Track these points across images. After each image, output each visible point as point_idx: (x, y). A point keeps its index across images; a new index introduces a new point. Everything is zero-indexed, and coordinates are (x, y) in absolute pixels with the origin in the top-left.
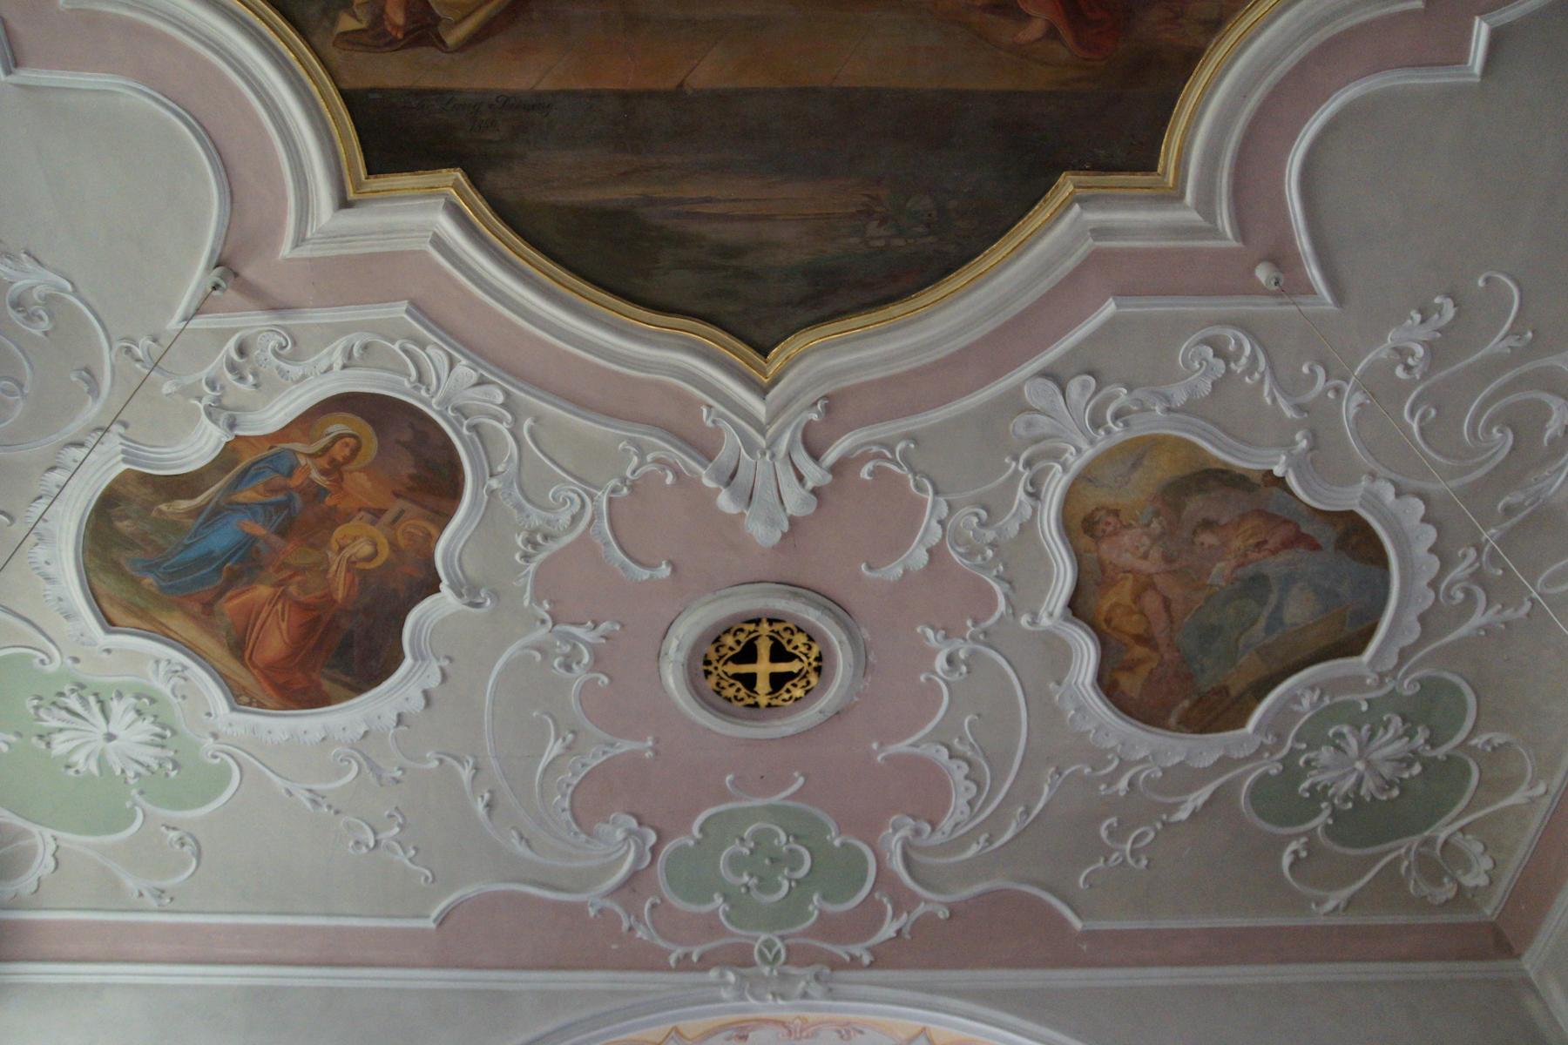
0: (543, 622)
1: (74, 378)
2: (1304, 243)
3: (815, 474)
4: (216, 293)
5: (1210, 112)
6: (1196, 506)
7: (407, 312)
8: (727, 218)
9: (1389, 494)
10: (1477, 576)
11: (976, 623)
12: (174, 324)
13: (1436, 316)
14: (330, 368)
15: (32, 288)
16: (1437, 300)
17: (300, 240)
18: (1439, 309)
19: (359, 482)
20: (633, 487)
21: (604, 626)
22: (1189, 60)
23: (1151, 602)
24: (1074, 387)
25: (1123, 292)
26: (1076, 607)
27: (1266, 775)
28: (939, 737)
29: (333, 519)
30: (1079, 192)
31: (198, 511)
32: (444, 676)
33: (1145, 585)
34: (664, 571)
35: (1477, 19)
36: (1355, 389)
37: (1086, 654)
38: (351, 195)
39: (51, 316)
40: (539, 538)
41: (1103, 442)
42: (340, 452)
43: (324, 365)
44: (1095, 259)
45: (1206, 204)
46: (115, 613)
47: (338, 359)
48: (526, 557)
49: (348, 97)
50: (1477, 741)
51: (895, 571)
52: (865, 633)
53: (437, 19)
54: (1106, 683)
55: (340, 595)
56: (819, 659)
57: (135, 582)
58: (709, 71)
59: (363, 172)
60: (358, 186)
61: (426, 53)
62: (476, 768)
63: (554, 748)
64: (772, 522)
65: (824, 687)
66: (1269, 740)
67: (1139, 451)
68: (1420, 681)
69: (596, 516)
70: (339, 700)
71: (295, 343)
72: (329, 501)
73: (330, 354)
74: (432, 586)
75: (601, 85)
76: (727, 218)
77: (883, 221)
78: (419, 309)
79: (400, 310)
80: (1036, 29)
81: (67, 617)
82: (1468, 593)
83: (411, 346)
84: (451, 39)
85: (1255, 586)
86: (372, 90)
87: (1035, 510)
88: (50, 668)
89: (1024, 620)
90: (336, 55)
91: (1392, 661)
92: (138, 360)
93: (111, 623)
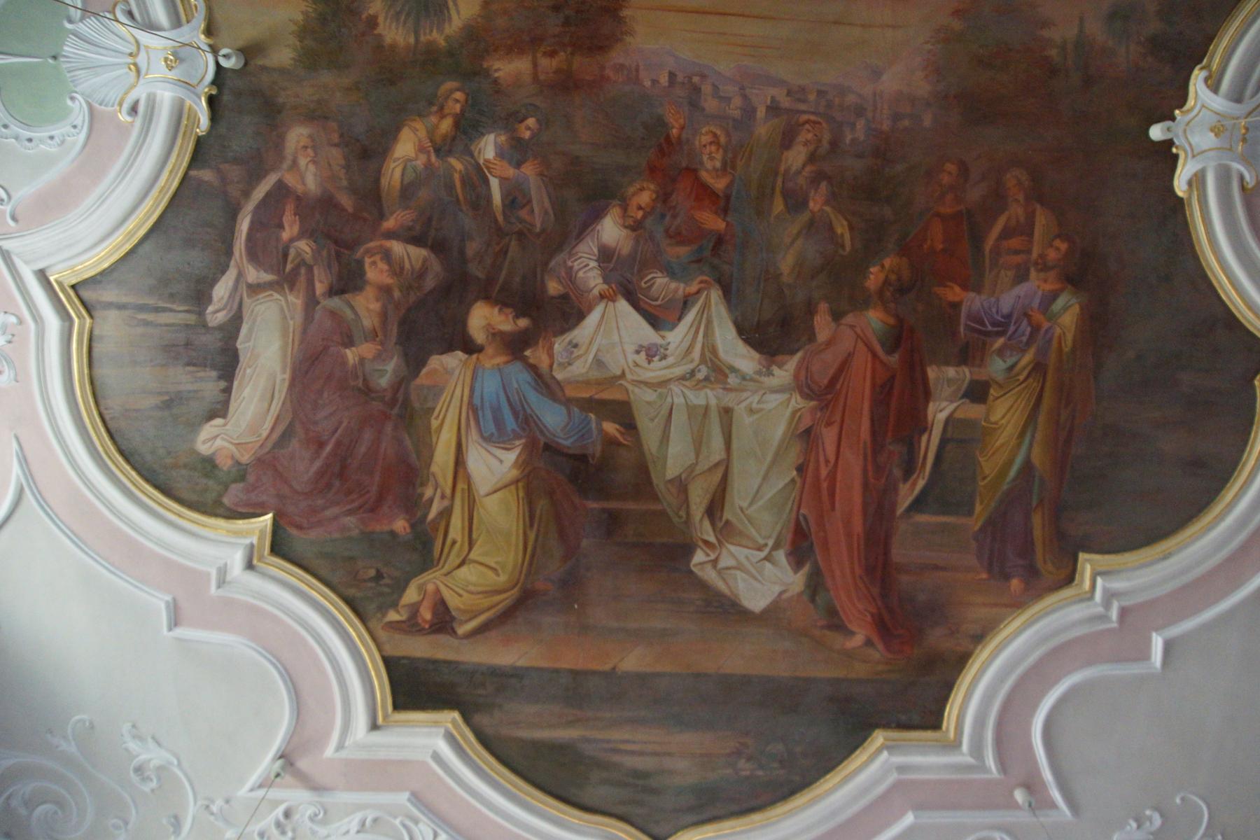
1: (164, 821)
2: (1047, 775)
4: (278, 779)
5: (975, 696)
7: (409, 800)
8: (641, 754)
13: (1148, 824)
14: (348, 832)
15: (150, 760)
16: (1148, 812)
17: (340, 746)
18: (1150, 819)
22: (962, 660)
25: (918, 807)
30: (889, 743)
35: (1154, 635)
38: (380, 720)
39: (159, 779)
43: (344, 829)
44: (897, 786)
45: (977, 749)
47: (354, 826)
49: (387, 661)
53: (453, 619)
58: (633, 661)
59: (390, 708)
60: (386, 717)
61: (443, 638)
71: (325, 813)
73: (350, 822)
75: (557, 665)
76: (641, 754)
77: (749, 759)
78: (416, 798)
79: (403, 798)
80: (858, 640)
84: (461, 630)
86: (403, 658)
90: (383, 635)
92: (212, 814)
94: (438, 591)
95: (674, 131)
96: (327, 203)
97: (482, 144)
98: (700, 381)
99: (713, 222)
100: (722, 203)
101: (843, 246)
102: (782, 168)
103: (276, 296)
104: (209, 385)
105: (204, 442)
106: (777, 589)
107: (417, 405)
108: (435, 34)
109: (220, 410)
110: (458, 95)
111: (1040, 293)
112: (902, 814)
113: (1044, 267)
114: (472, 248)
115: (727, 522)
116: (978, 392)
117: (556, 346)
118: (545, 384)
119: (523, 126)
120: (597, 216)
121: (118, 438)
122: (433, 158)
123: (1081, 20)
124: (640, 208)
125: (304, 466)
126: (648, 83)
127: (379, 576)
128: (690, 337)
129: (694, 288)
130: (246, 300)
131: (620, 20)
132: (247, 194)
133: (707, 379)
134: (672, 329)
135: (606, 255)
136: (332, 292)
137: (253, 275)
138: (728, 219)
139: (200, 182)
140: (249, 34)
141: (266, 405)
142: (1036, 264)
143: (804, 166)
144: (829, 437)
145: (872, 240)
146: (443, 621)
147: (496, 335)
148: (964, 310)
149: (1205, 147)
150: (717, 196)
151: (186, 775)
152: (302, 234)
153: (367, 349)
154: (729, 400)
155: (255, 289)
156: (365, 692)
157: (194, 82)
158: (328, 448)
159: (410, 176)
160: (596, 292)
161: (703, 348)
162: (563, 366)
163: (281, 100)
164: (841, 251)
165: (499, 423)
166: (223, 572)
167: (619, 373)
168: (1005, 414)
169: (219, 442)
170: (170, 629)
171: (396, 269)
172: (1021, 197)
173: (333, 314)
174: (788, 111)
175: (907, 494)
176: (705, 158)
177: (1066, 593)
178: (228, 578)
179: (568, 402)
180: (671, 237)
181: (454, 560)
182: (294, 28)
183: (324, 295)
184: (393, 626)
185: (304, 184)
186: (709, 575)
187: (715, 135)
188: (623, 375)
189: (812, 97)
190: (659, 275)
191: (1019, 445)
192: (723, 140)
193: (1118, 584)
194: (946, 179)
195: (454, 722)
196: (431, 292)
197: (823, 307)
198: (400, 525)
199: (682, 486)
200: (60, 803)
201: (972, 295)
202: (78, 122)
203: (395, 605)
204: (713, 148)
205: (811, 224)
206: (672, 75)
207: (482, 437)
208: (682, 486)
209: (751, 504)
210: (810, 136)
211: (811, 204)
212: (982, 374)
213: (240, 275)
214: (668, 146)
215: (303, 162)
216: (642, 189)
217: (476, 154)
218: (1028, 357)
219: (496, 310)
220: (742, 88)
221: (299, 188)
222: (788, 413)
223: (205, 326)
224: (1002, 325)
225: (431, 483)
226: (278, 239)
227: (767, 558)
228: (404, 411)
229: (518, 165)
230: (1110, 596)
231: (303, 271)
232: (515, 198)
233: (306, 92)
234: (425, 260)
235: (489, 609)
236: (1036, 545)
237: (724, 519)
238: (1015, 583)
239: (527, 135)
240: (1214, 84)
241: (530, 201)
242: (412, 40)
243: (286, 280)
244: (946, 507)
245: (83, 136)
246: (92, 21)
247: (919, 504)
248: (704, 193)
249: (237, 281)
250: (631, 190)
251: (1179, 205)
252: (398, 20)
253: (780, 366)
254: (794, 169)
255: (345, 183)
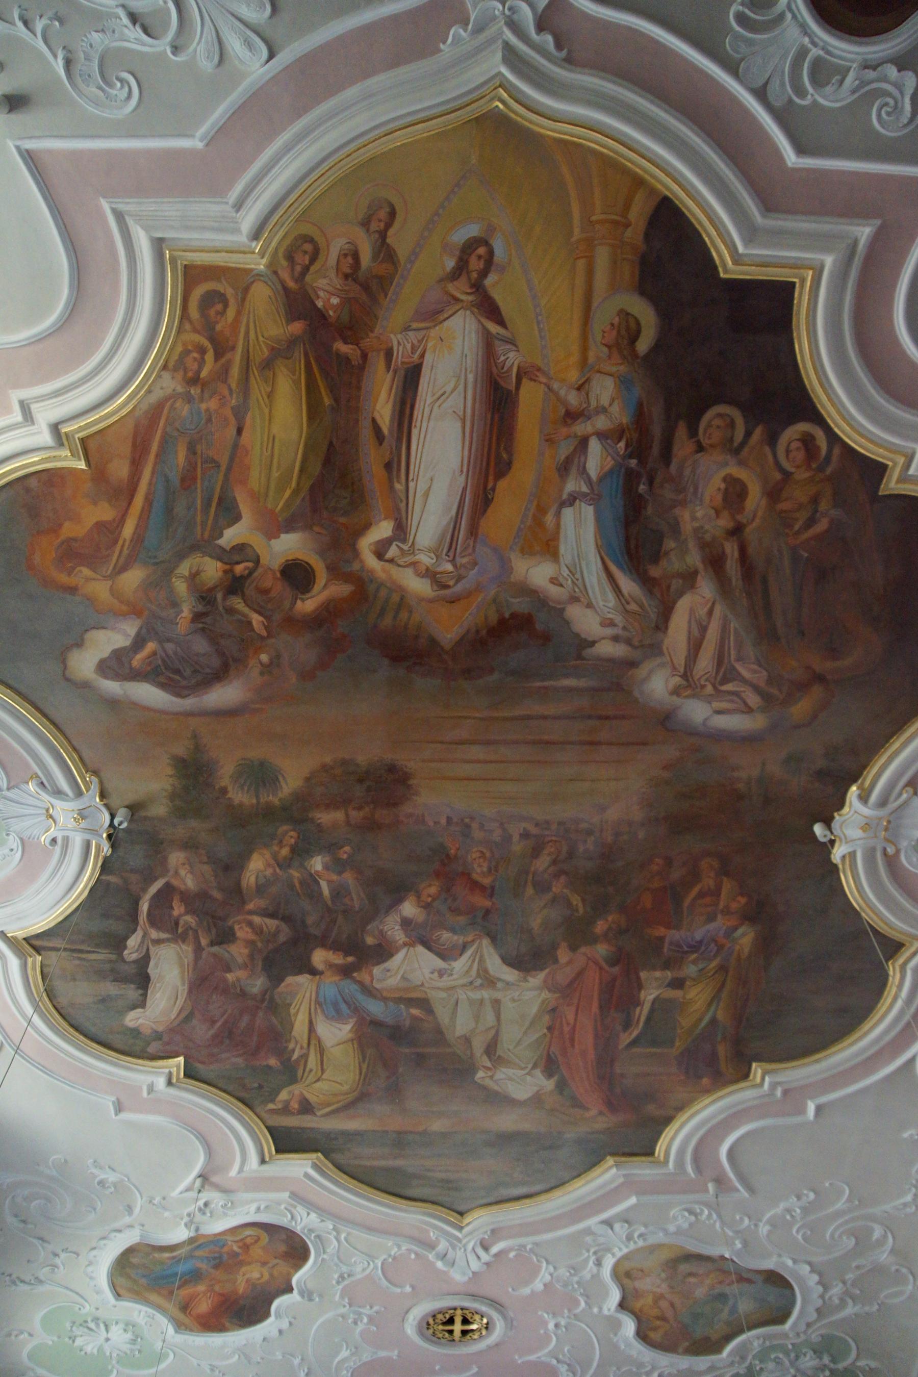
0: (344, 1306)
3: (485, 1257)
6: (684, 1268)
9: (790, 1263)
10: (846, 1293)
11: (569, 1311)
12: (175, 1193)
17: (241, 1170)
18: (807, 1195)
19: (257, 1252)
20: (394, 1258)
21: (376, 1308)
23: (664, 1304)
24: (617, 1226)
25: (638, 1194)
26: (623, 1305)
27: (738, 1374)
28: (552, 1354)
29: (241, 1263)
31: (174, 1258)
32: (291, 1323)
33: (658, 1298)
34: (408, 1289)
36: (764, 1225)
37: (629, 1326)
38: (267, 1159)
40: (346, 1275)
41: (632, 1246)
42: (248, 1241)
46: (121, 1292)
48: (338, 1283)
49: (270, 1130)
50: (858, 1364)
51: (527, 1291)
52: (511, 1314)
54: (642, 1335)
55: (241, 1292)
56: (487, 1324)
57: (135, 1281)
62: (302, 1359)
63: (345, 1353)
64: (464, 1274)
65: (488, 1336)
66: (737, 1359)
67: (653, 1249)
68: (822, 1336)
69: (376, 1268)
70: (233, 1330)
72: (241, 1258)
74: (290, 1290)
80: (594, 1112)
81: (97, 1293)
82: (842, 1300)
83: (290, 1208)
84: (319, 1113)
85: (722, 1297)
87: (598, 1271)
88: (83, 1311)
89: (595, 1310)
91: (803, 1327)
93: (119, 1295)
94: (302, 1094)
95: (452, 851)
96: (203, 895)
97: (312, 862)
98: (476, 987)
99: (482, 902)
100: (489, 892)
101: (577, 911)
102: (533, 869)
103: (173, 945)
104: (132, 993)
105: (131, 1020)
106: (535, 1089)
107: (279, 1001)
108: (271, 798)
109: (141, 1004)
110: (292, 833)
111: (725, 928)
112: (627, 1198)
113: (727, 912)
114: (310, 920)
115: (499, 1056)
116: (678, 984)
117: (374, 971)
118: (369, 991)
119: (342, 850)
120: (400, 901)
121: (67, 1017)
122: (278, 870)
123: (764, 764)
124: (429, 896)
125: (202, 1032)
126: (431, 824)
127: (261, 1087)
128: (469, 963)
129: (470, 939)
130: (151, 947)
131: (409, 787)
132: (144, 890)
133: (481, 985)
134: (456, 960)
135: (406, 923)
136: (212, 944)
137: (154, 934)
138: (494, 900)
139: (108, 884)
140: (131, 798)
141: (172, 1002)
142: (722, 911)
143: (549, 866)
144: (569, 1014)
145: (599, 907)
146: (306, 1108)
147: (331, 966)
148: (667, 940)
149: (855, 837)
150: (485, 888)
151: (134, 1186)
152: (187, 912)
153: (241, 974)
154: (498, 995)
155: (158, 942)
156: (256, 1147)
157: (97, 828)
158: (219, 1024)
159: (262, 881)
160: (401, 942)
161: (478, 970)
162: (379, 981)
163: (161, 837)
164: (576, 914)
165: (338, 1011)
166: (151, 1088)
167: (420, 983)
168: (697, 996)
169: (140, 1021)
170: (116, 1115)
171: (258, 931)
172: (712, 874)
173: (215, 955)
174: (535, 836)
175: (626, 1039)
176: (475, 866)
177: (742, 1085)
178: (155, 1089)
179: (385, 999)
180: (452, 911)
181: (311, 1078)
182: (165, 794)
183: (208, 946)
184: (273, 1111)
185: (185, 884)
186: (488, 1082)
187: (482, 852)
188: (422, 985)
189: (554, 827)
190: (445, 932)
191: (707, 1010)
192: (488, 855)
193: (780, 1078)
194: (655, 868)
195: (318, 1158)
196: (284, 943)
197: (564, 945)
198: (273, 1062)
199: (467, 1040)
200: (49, 1200)
201: (673, 932)
202: (14, 846)
203: (272, 1101)
204: (481, 860)
205: (554, 900)
206: (449, 820)
207: (327, 1017)
208: (467, 1040)
209: (515, 1047)
210: (552, 850)
211: (554, 889)
212: (681, 974)
213: (145, 935)
214: (447, 859)
215: (182, 872)
216: (430, 885)
217: (309, 868)
218: (714, 964)
219: (331, 952)
220: (502, 824)
221: (183, 887)
222: (540, 1001)
223: (124, 961)
224: (695, 947)
225: (293, 1041)
226: (170, 916)
227: (528, 1074)
228: (272, 1004)
229: (340, 873)
230: (773, 1086)
231: (191, 933)
232: (338, 892)
233: (180, 831)
234: (277, 927)
235: (338, 1102)
236: (724, 1057)
237: (498, 1054)
238: (705, 1081)
239: (345, 856)
240: (864, 798)
241: (350, 894)
242: (254, 801)
243: (177, 934)
244: (654, 1043)
245: (19, 855)
246: (16, 791)
247: (634, 1043)
248: (475, 886)
249: (144, 937)
250: (423, 885)
251: (834, 869)
252: (243, 789)
253: (534, 977)
254: (541, 869)
255: (215, 884)
